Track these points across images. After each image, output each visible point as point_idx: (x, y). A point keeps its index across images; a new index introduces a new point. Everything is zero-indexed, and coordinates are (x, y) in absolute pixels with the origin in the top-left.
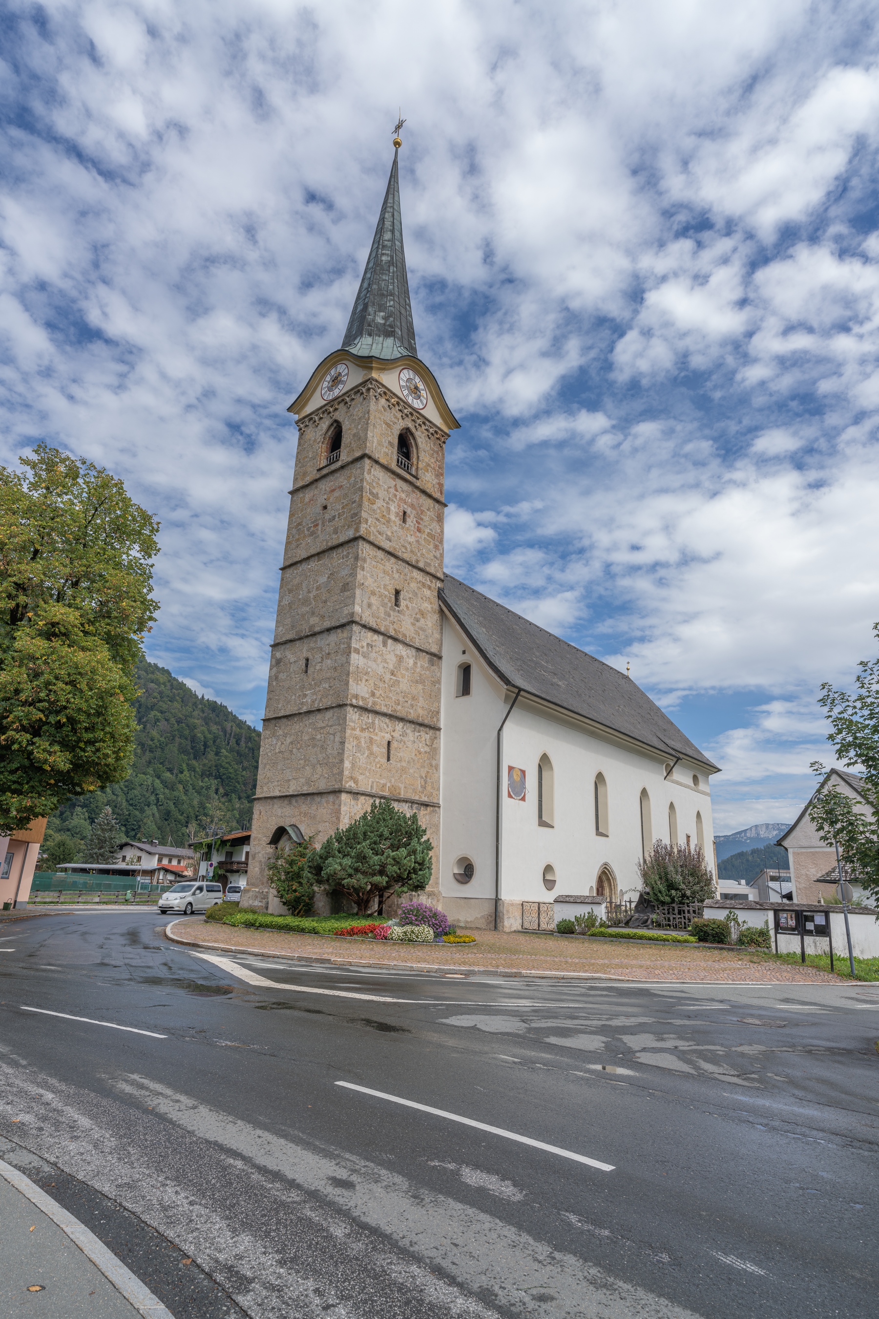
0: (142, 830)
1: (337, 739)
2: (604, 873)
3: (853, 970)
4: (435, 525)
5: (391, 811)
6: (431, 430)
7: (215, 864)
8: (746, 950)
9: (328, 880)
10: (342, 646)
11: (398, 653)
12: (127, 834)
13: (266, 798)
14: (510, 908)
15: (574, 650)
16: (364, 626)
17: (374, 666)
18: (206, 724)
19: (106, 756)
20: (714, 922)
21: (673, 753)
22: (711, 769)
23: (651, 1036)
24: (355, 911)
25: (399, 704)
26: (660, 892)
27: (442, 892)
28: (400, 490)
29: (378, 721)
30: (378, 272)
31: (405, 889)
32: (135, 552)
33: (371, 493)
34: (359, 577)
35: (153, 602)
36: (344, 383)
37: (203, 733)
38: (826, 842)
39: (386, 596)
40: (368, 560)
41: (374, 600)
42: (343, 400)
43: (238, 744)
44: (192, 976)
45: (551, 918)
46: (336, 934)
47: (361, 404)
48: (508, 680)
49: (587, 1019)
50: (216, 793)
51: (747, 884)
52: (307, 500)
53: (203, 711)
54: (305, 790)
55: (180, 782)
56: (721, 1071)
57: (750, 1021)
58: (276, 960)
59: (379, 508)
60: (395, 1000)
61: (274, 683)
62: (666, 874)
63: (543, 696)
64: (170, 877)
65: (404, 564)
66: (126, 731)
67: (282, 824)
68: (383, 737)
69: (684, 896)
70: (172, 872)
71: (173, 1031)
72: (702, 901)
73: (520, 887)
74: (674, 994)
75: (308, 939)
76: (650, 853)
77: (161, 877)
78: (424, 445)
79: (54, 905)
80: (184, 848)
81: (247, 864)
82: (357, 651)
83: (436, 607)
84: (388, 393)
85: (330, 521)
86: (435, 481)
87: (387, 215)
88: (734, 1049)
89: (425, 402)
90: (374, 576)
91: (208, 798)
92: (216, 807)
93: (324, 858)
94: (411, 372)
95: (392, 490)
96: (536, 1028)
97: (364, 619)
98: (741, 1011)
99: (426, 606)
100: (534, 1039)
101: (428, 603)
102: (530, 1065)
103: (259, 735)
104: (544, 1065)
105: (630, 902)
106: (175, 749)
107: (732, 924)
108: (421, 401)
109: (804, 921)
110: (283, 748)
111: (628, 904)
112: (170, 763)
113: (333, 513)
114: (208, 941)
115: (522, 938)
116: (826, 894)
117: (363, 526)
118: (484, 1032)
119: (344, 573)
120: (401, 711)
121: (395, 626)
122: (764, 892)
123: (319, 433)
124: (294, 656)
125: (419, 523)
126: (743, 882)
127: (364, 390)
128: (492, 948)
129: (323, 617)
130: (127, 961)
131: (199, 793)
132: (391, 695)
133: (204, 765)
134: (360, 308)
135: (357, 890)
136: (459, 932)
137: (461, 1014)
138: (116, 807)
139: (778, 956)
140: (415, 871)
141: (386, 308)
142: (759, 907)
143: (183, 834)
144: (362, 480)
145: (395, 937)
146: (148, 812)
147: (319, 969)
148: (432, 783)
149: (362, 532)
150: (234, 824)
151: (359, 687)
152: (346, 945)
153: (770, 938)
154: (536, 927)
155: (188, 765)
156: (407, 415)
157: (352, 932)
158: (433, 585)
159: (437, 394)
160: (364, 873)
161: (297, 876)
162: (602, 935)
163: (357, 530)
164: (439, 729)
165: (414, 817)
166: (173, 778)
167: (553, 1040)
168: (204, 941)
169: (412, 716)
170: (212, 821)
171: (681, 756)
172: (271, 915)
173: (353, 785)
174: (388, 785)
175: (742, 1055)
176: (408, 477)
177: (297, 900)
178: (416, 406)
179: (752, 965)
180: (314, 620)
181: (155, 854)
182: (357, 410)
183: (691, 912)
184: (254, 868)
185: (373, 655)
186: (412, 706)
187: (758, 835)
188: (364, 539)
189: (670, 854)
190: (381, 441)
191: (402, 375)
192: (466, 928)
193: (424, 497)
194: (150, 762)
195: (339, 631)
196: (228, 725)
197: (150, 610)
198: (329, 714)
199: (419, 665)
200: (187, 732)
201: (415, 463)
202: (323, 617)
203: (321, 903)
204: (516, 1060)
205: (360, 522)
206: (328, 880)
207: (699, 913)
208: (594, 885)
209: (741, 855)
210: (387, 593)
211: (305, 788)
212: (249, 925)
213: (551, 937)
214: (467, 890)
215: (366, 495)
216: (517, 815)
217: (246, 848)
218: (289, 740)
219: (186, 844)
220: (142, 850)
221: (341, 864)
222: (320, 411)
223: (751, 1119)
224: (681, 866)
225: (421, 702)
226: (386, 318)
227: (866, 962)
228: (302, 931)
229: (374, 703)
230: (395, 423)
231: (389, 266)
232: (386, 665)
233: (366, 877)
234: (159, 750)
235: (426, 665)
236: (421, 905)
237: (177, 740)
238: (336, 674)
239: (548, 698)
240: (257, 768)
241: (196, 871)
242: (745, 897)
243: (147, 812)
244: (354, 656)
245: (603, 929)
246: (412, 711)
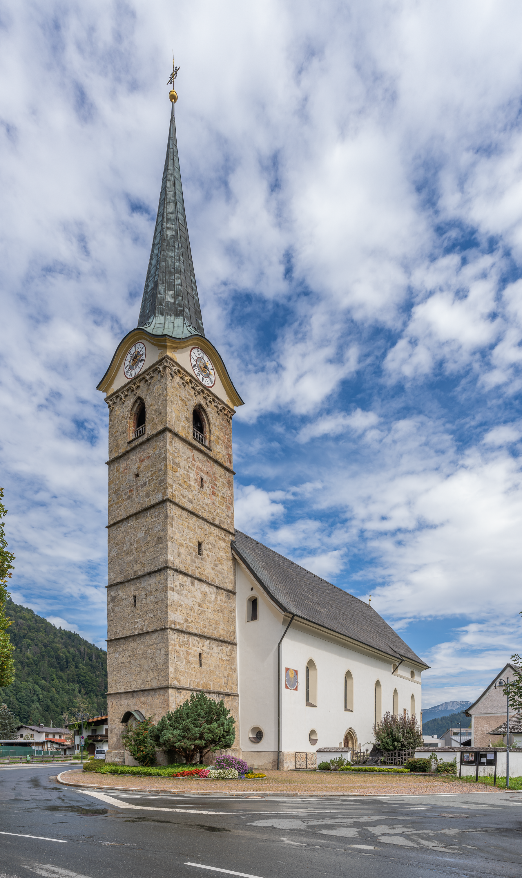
0: (31, 717)
1: (163, 652)
2: (349, 733)
3: (508, 784)
4: (226, 490)
5: (205, 699)
6: (220, 407)
7: (85, 737)
8: (441, 775)
9: (164, 744)
10: (161, 586)
11: (203, 590)
12: (21, 720)
13: (115, 693)
14: (288, 757)
15: (332, 587)
16: (176, 570)
17: (186, 600)
18: (65, 647)
20: (421, 760)
21: (399, 657)
22: (424, 667)
23: (386, 827)
24: (185, 762)
25: (206, 627)
26: (387, 744)
27: (242, 748)
28: (196, 459)
29: (192, 640)
30: (164, 247)
31: (218, 748)
33: (174, 462)
34: (170, 532)
35: (9, 553)
37: (64, 653)
38: (513, 708)
39: (191, 547)
40: (176, 519)
41: (182, 550)
42: (143, 378)
43: (90, 659)
44: (79, 804)
45: (315, 761)
46: (173, 776)
47: (160, 382)
48: (285, 608)
49: (343, 818)
50: (80, 693)
51: (438, 737)
52: (122, 469)
53: (62, 639)
54: (143, 687)
55: (52, 687)
56: (434, 844)
57: (446, 815)
58: (134, 792)
59: (181, 475)
60: (217, 813)
61: (112, 615)
62: (392, 733)
63: (310, 619)
64: (56, 746)
65: (203, 522)
66: (5, 650)
67: (128, 710)
68: (196, 650)
69: (403, 745)
70: (56, 743)
71: (70, 838)
72: (414, 748)
73: (294, 743)
74: (396, 802)
75: (154, 779)
76: (381, 720)
77: (49, 746)
78: (215, 420)
80: (62, 728)
81: (107, 736)
82: (172, 589)
83: (230, 555)
84: (181, 371)
85: (142, 486)
86: (225, 452)
87: (169, 184)
88: (439, 832)
89: (213, 380)
90: (180, 534)
91: (74, 696)
92: (81, 702)
93: (160, 730)
94: (200, 351)
95: (191, 460)
96: (312, 826)
97: (175, 565)
98: (439, 810)
99: (222, 555)
100: (312, 832)
101: (224, 553)
102: (311, 847)
103: (105, 653)
104: (320, 846)
105: (367, 750)
106: (46, 665)
107: (433, 761)
108: (210, 379)
109: (479, 758)
110: (124, 660)
111: (365, 752)
112: (43, 674)
113: (144, 480)
114: (87, 783)
115: (296, 774)
116: (492, 742)
117: (169, 491)
118: (279, 829)
119: (157, 529)
120: (207, 632)
121: (200, 570)
122: (448, 742)
123: (125, 410)
124: (125, 594)
125: (214, 488)
126: (436, 736)
127: (161, 368)
128: (277, 780)
129: (144, 564)
130: (33, 797)
131: (67, 693)
132: (199, 621)
133: (68, 675)
134: (151, 286)
135: (184, 750)
136: (255, 772)
137: (262, 819)
138: (10, 704)
139: (460, 778)
140: (224, 736)
141: (174, 286)
142: (451, 750)
143: (60, 719)
144: (165, 451)
145: (213, 776)
146: (33, 706)
147: (164, 797)
148: (232, 680)
149: (169, 495)
150: (95, 712)
151: (176, 615)
152: (181, 782)
153: (456, 768)
154: (305, 767)
155: (56, 675)
156: (198, 392)
157: (183, 774)
158: (227, 539)
159: (223, 372)
160: (188, 739)
161: (143, 742)
162: (348, 770)
163: (165, 493)
164: (236, 644)
165: (221, 703)
166: (47, 684)
167: (324, 832)
168: (84, 783)
169: (216, 635)
170: (79, 711)
171: (405, 659)
172: (128, 766)
173: (177, 683)
174: (202, 682)
175: (445, 835)
176: (203, 448)
177: (145, 757)
178: (206, 384)
179: (444, 783)
180: (137, 567)
181: (43, 732)
182: (157, 389)
183: (407, 754)
184: (113, 739)
185: (184, 592)
186: (215, 628)
187: (447, 708)
188: (171, 501)
189: (394, 721)
190: (178, 416)
191: (192, 354)
192: (259, 769)
193: (217, 466)
194: (29, 674)
195: (157, 574)
196: (82, 647)
197: (7, 560)
198: (155, 636)
199: (219, 599)
200: (52, 653)
201: (208, 436)
202: (144, 564)
203: (161, 758)
204: (302, 844)
205: (166, 487)
206: (164, 744)
207: (412, 755)
208: (342, 740)
209: (435, 720)
210: (191, 545)
211: (143, 686)
212: (114, 773)
213: (315, 772)
214: (260, 747)
215: (170, 464)
216: (292, 699)
217: (105, 727)
218: (127, 654)
219: (63, 725)
220: (33, 730)
221: (172, 734)
222: (125, 389)
223: (457, 871)
224: (402, 728)
225: (222, 626)
226: (175, 297)
227: (516, 779)
228: (150, 775)
229: (188, 627)
230: (189, 400)
231: (174, 242)
232: (194, 599)
233: (193, 739)
234: (34, 665)
235: (224, 599)
236: (229, 756)
237: (46, 659)
238: (158, 607)
239: (314, 621)
240: (106, 675)
241: (73, 742)
242: (436, 745)
243: (33, 706)
244: (170, 593)
245: (348, 767)
246: (215, 632)
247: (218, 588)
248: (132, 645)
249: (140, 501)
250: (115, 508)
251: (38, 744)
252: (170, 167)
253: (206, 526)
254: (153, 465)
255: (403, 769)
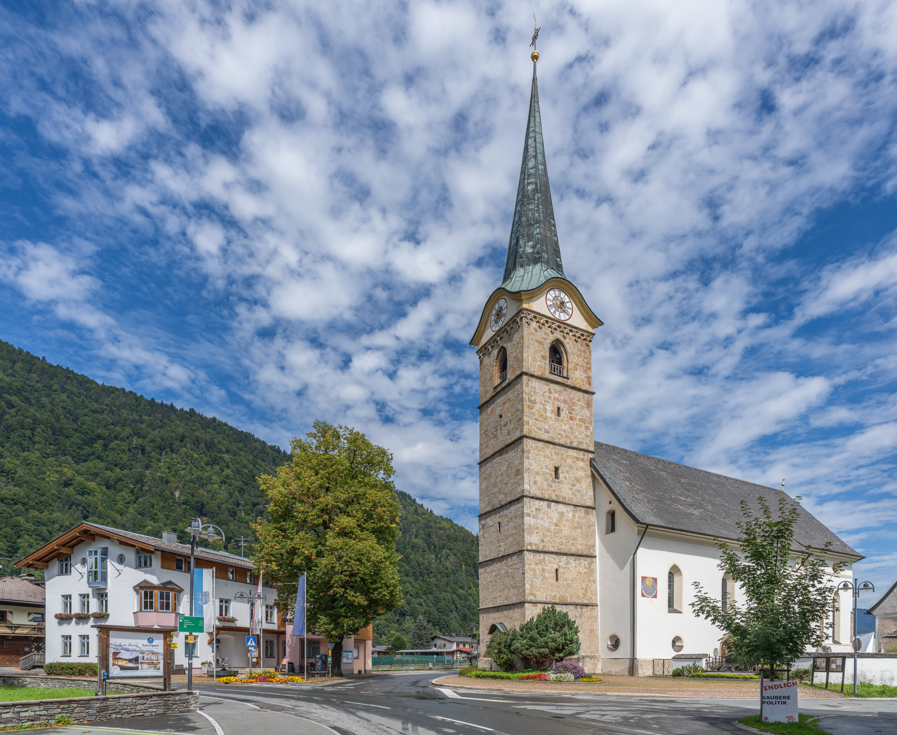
1: (521, 572)
6: (577, 335)
16: (532, 498)
17: (542, 522)
19: (385, 595)
28: (553, 391)
29: (547, 557)
32: (381, 475)
36: (505, 315)
41: (538, 478)
64: (464, 655)
79: (383, 670)
83: (589, 473)
84: (537, 315)
89: (570, 312)
95: (547, 394)
99: (581, 473)
106: (463, 574)
119: (516, 462)
120: (564, 549)
134: (514, 241)
146: (452, 616)
149: (526, 431)
157: (528, 678)
159: (580, 302)
163: (522, 431)
164: (595, 557)
177: (505, 663)
178: (563, 318)
180: (501, 497)
188: (527, 437)
198: (514, 558)
200: (469, 561)
212: (478, 676)
214: (616, 654)
218: (494, 574)
225: (580, 540)
229: (544, 546)
233: (545, 647)
244: (526, 519)
247: (575, 506)
248: (497, 565)
249: (504, 439)
250: (484, 447)
251: (448, 653)
252: (532, 125)
253: (564, 450)
254: (513, 406)
255: (752, 675)
